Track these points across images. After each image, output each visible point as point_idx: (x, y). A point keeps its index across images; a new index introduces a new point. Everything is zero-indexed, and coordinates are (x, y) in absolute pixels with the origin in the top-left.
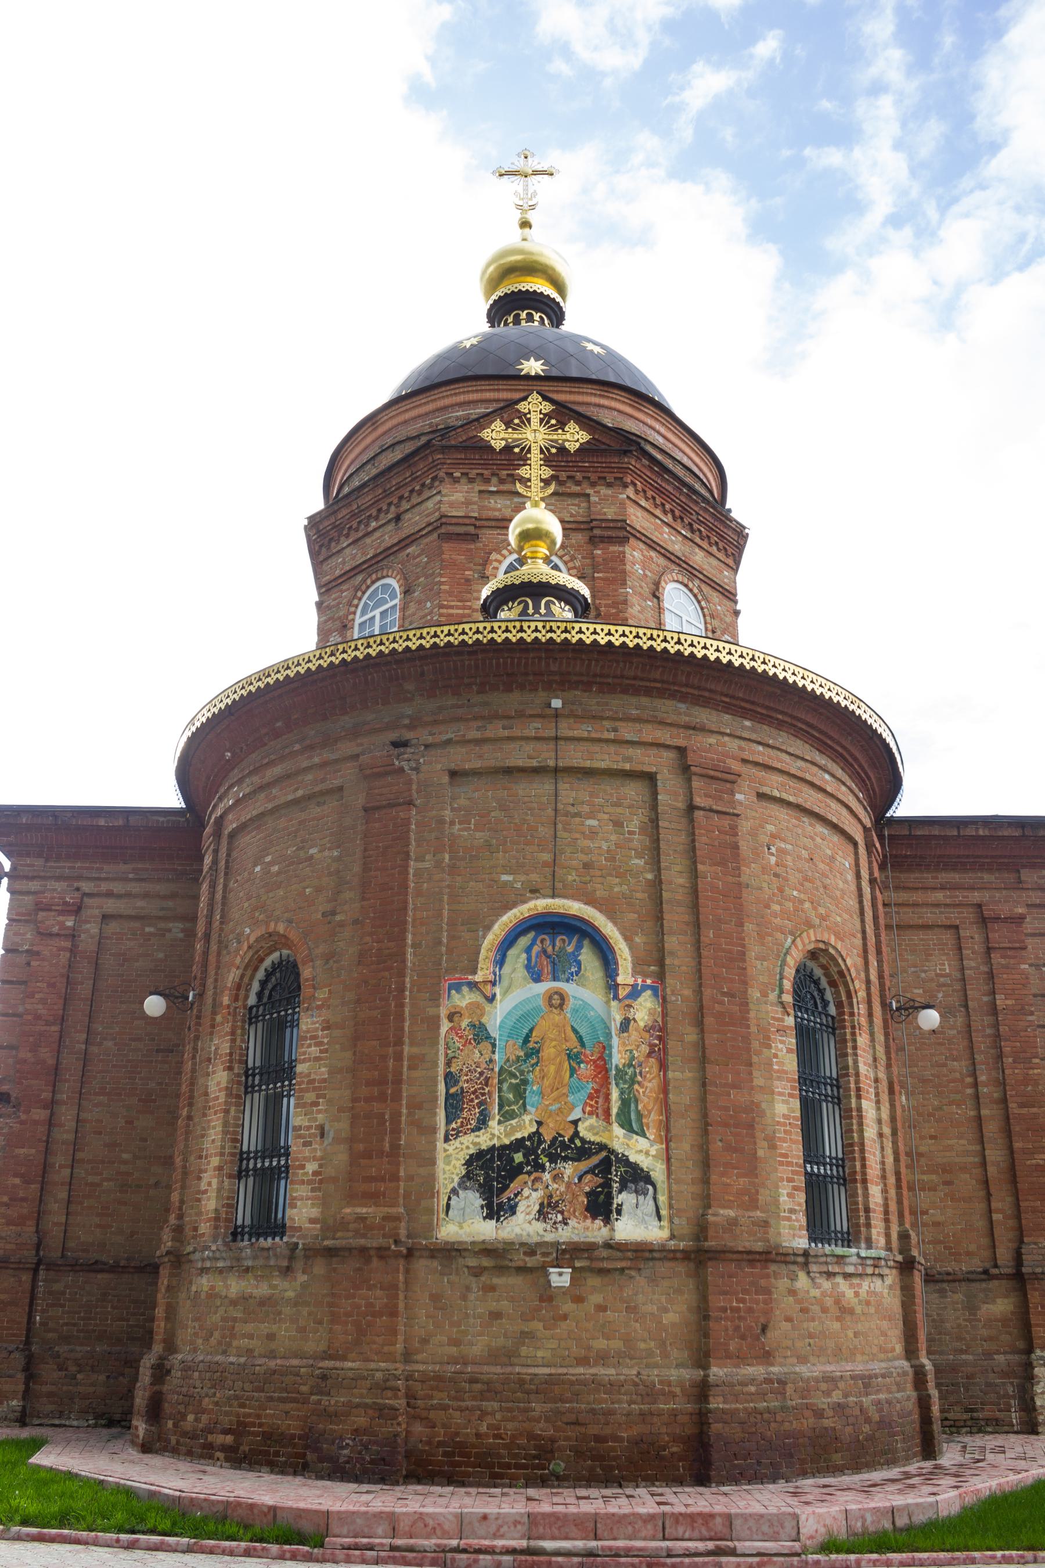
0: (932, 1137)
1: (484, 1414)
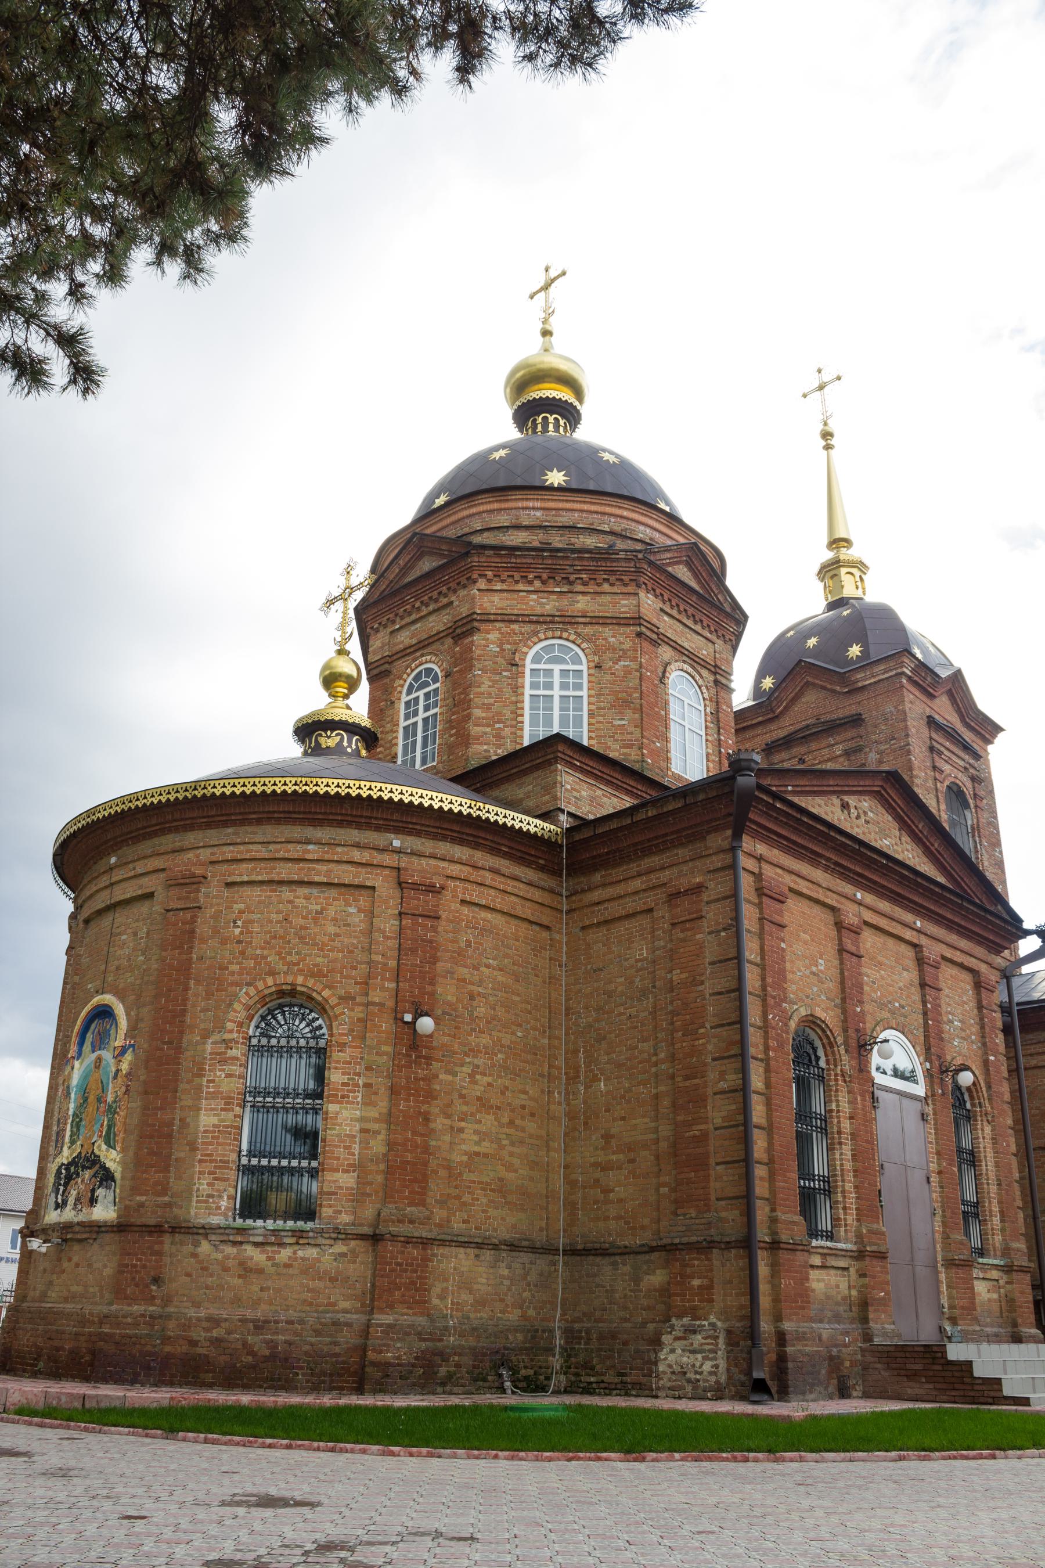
0: (623, 1119)
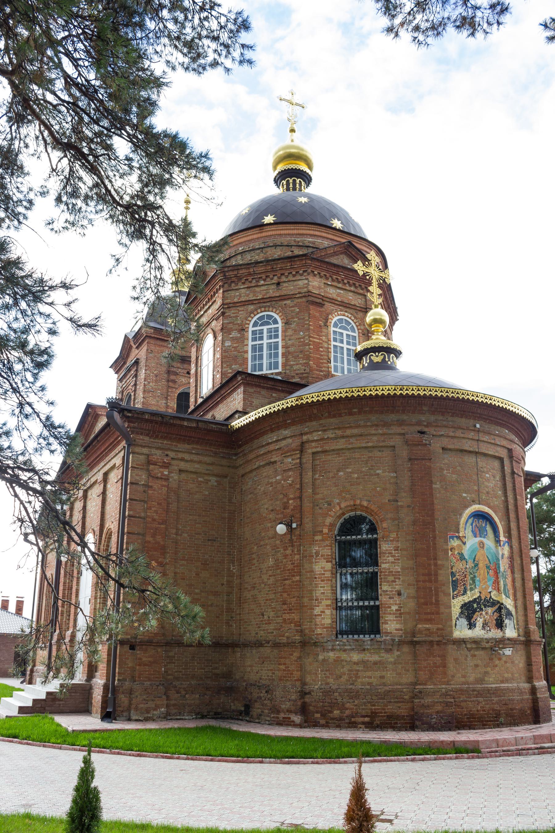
1: (479, 703)
